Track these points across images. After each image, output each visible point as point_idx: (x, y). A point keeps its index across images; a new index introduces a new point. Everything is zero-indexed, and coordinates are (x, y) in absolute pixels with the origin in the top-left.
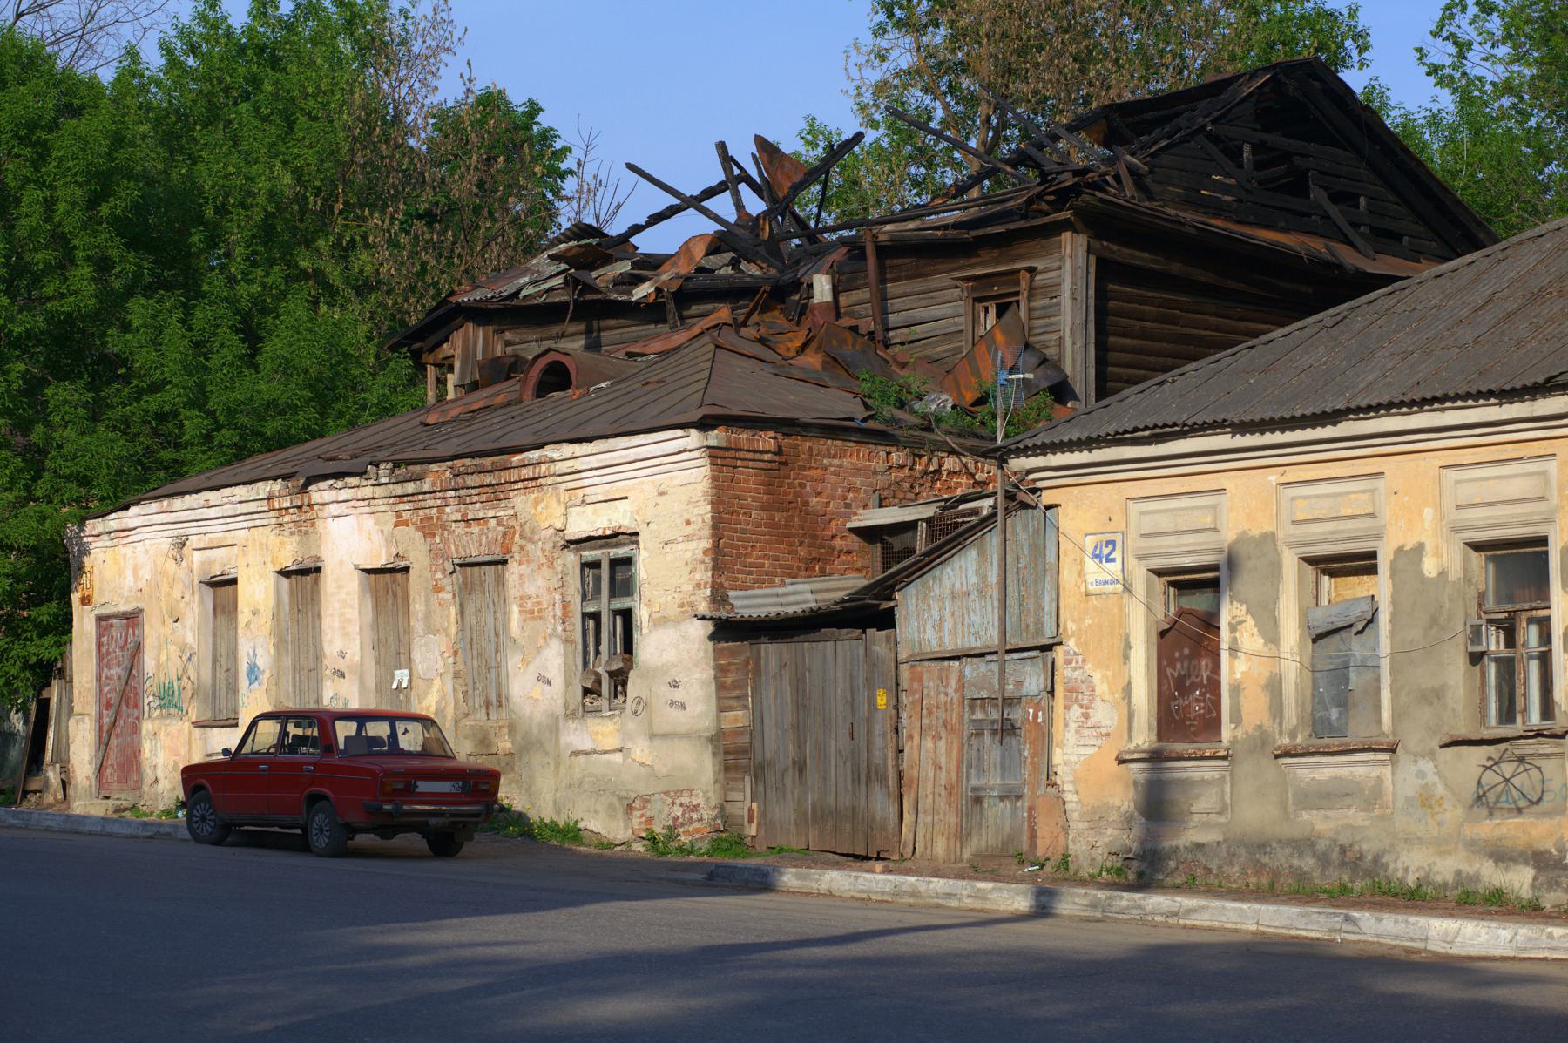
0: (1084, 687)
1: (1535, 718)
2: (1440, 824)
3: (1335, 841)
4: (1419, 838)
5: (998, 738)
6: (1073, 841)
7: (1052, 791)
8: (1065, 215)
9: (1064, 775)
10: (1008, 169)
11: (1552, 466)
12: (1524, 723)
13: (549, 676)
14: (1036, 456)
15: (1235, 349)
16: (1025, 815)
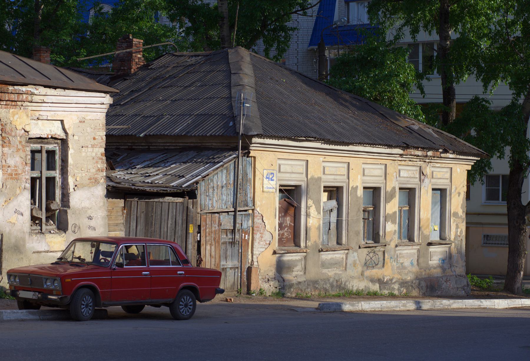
13: (22, 211)
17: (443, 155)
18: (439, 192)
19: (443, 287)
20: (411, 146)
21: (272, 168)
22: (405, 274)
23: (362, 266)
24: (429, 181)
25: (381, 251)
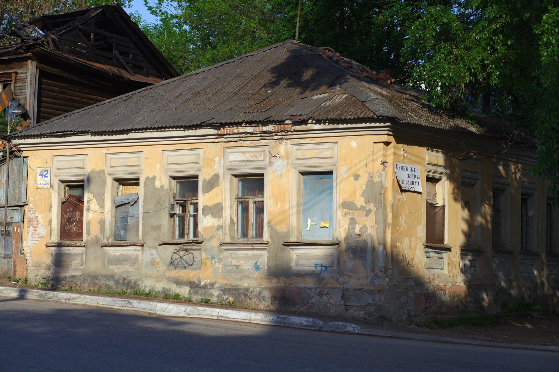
0: (35, 220)
1: (191, 236)
2: (158, 271)
3: (121, 276)
4: (150, 276)
5: (4, 237)
6: (29, 273)
7: (22, 256)
8: (29, 54)
9: (27, 250)
10: (8, 36)
11: (201, 152)
12: (187, 238)
14: (21, 139)
15: (92, 106)
16: (12, 264)
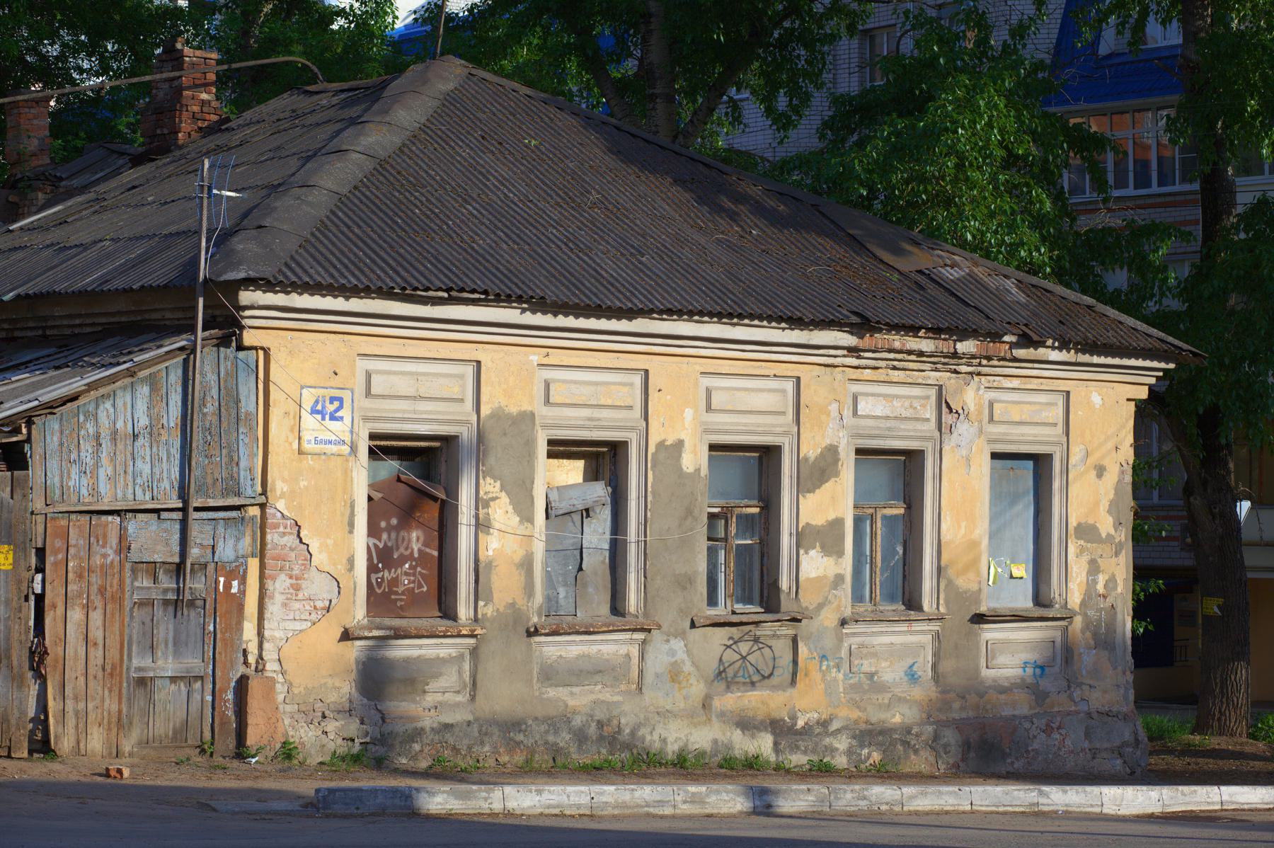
3: (591, 716)
17: (1020, 353)
18: (1030, 464)
19: (1036, 745)
20: (878, 322)
21: (336, 382)
22: (880, 706)
23: (706, 681)
24: (974, 429)
25: (786, 635)
